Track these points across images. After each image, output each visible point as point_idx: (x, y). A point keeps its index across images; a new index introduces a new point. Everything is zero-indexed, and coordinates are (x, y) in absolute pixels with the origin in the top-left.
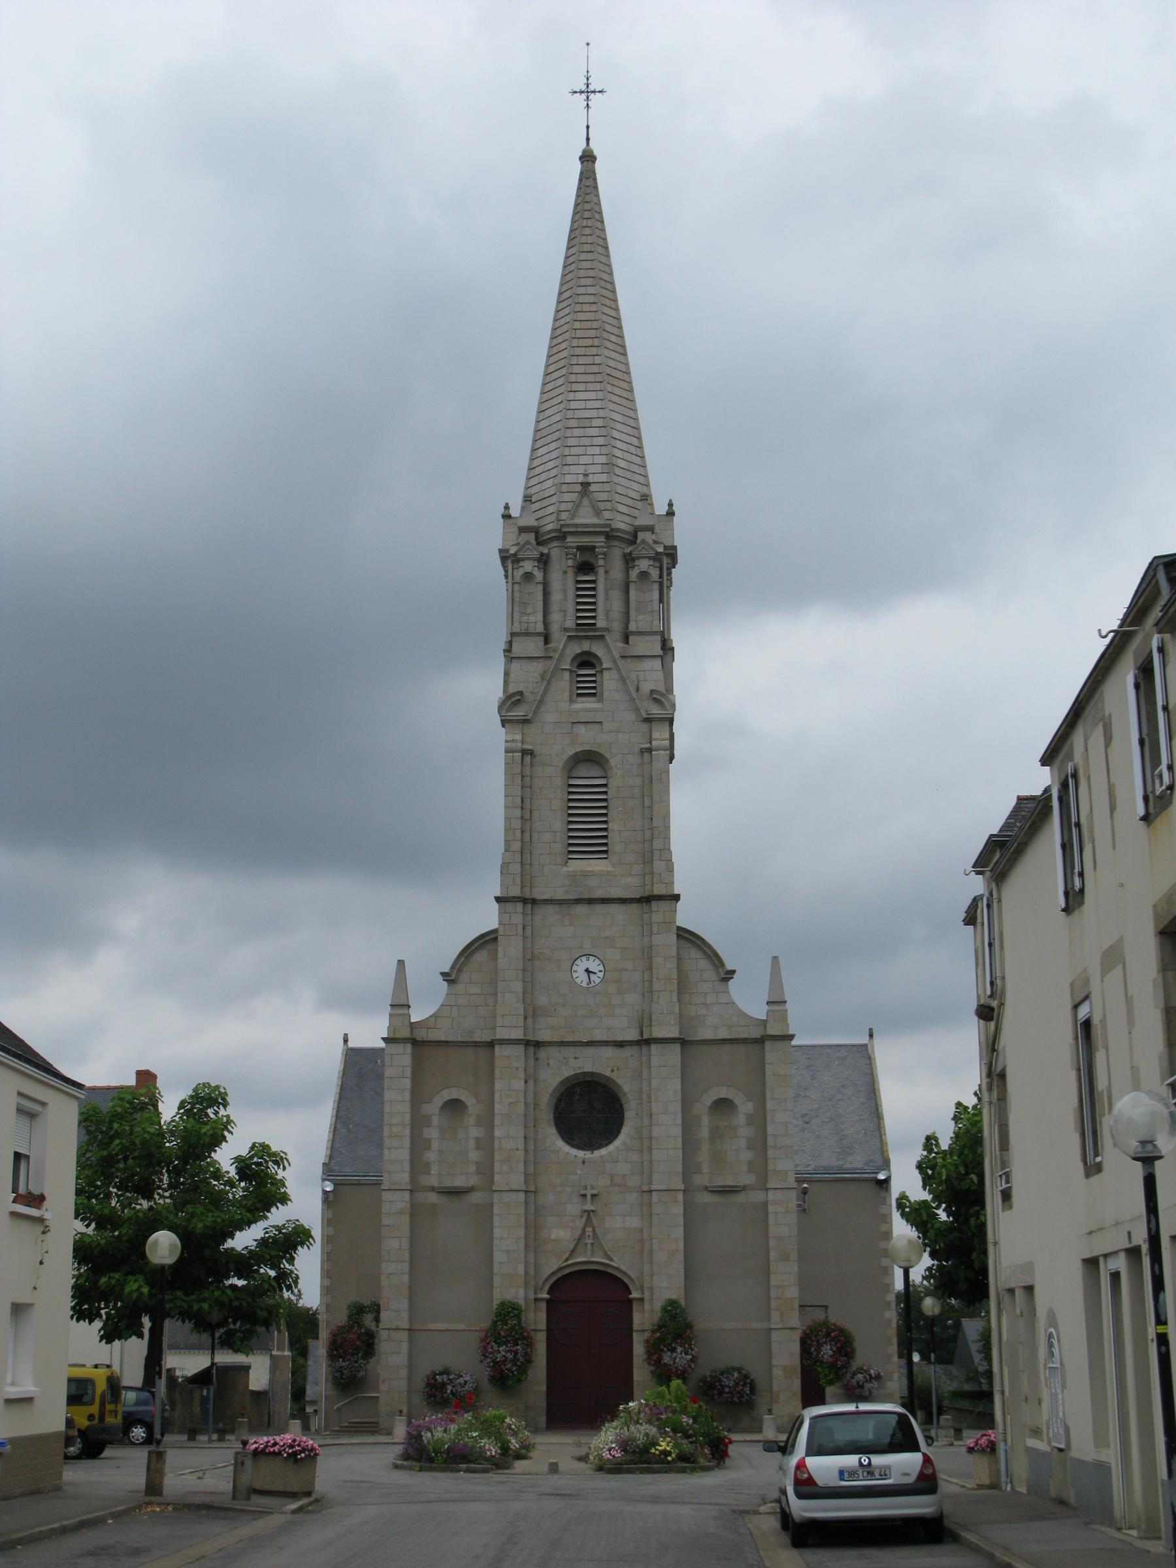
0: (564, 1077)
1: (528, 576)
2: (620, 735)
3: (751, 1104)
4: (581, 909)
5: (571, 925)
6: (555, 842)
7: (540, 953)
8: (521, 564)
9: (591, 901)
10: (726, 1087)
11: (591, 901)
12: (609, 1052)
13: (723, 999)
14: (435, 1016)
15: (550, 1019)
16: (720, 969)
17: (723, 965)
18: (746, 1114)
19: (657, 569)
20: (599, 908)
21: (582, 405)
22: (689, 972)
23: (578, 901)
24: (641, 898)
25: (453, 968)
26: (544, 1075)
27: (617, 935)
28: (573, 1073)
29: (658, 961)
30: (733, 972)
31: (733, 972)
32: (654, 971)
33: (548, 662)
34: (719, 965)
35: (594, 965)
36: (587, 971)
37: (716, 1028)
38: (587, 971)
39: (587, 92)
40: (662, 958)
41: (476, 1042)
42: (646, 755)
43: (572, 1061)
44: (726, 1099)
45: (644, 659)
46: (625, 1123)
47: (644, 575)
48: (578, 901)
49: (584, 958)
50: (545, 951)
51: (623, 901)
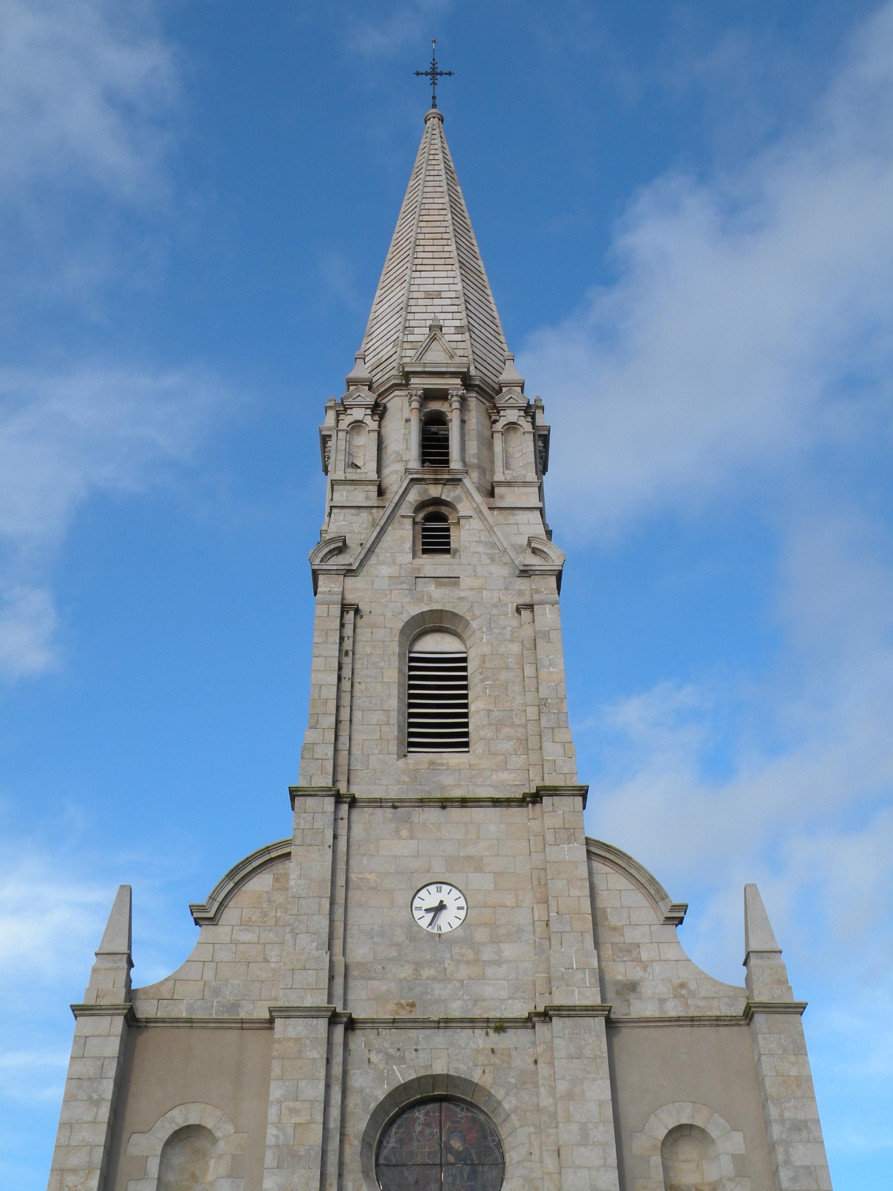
0: (395, 1085)
1: (357, 425)
2: (485, 593)
3: (738, 1137)
4: (433, 814)
5: (411, 838)
6: (388, 724)
7: (361, 879)
8: (349, 412)
9: (444, 803)
10: (691, 1105)
11: (444, 803)
12: (480, 1040)
13: (670, 953)
14: (174, 979)
15: (374, 984)
16: (660, 904)
17: (664, 897)
18: (733, 1155)
19: (530, 424)
20: (455, 813)
21: (431, 189)
22: (608, 910)
23: (422, 803)
24: (525, 796)
25: (212, 898)
26: (359, 1080)
27: (486, 853)
28: (414, 1076)
29: (558, 885)
30: (684, 908)
31: (684, 908)
32: (553, 903)
33: (381, 511)
34: (657, 897)
35: (450, 921)
36: (442, 907)
37: (662, 1001)
38: (442, 907)
39: (434, 73)
40: (565, 881)
41: (242, 1021)
42: (525, 614)
43: (410, 1055)
44: (691, 1127)
45: (515, 512)
46: (508, 1175)
47: (512, 426)
48: (422, 803)
49: (432, 888)
50: (367, 876)
51: (496, 802)
